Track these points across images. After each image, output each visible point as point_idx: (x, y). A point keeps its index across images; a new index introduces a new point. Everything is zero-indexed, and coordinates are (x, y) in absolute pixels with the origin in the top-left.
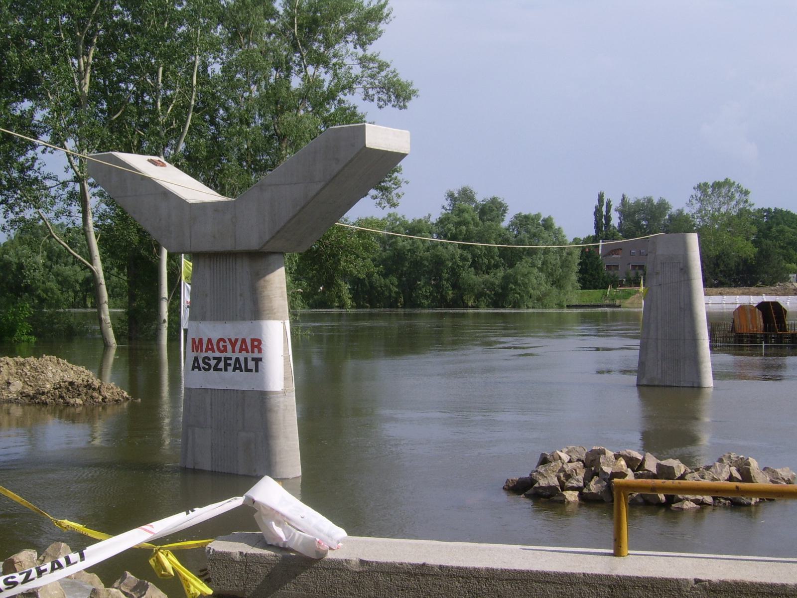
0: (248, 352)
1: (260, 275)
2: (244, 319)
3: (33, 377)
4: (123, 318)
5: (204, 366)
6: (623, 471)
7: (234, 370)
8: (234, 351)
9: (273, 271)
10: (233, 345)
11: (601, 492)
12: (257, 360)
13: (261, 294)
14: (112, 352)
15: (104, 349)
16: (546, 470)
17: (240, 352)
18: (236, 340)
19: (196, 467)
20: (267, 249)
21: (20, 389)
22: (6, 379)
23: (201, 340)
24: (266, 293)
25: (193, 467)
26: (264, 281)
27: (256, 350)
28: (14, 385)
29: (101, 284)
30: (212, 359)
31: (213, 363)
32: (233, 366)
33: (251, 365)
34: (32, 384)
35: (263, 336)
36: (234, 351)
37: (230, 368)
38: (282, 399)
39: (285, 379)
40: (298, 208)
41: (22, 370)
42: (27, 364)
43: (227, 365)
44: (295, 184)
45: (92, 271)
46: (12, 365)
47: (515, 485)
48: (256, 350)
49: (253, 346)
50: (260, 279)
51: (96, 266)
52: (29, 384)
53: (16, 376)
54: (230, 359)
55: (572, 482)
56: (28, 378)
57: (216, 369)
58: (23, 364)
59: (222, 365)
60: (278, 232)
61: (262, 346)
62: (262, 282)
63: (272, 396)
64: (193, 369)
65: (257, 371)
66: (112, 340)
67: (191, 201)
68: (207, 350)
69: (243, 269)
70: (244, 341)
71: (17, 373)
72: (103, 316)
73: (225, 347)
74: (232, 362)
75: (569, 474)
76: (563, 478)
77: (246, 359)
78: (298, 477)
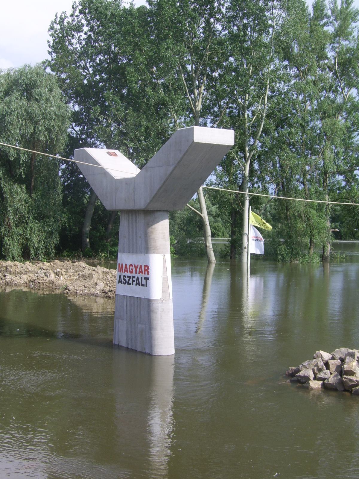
0: (142, 274)
1: (149, 225)
2: (141, 253)
3: (112, 281)
4: (228, 246)
5: (123, 281)
6: (352, 370)
7: (136, 285)
8: (136, 273)
9: (158, 222)
10: (136, 269)
11: (336, 383)
12: (147, 279)
13: (150, 237)
14: (213, 266)
15: (208, 264)
16: (308, 364)
17: (139, 273)
18: (138, 265)
19: (120, 344)
20: (152, 207)
21: (102, 288)
22: (96, 281)
23: (122, 264)
24: (153, 236)
25: (118, 344)
26: (152, 229)
27: (146, 272)
28: (99, 285)
29: (206, 225)
30: (127, 277)
31: (127, 279)
32: (136, 281)
33: (144, 282)
34: (110, 285)
35: (150, 263)
36: (136, 273)
37: (135, 283)
38: (160, 305)
39: (163, 292)
40: (162, 182)
41: (107, 277)
42: (109, 273)
43: (133, 281)
44: (161, 166)
45: (201, 216)
46: (101, 273)
47: (293, 373)
48: (146, 272)
49: (145, 270)
50: (150, 227)
51: (204, 214)
52: (109, 285)
53: (102, 280)
54: (134, 277)
55: (321, 374)
56: (109, 282)
57: (129, 284)
58: (107, 273)
59: (131, 281)
60: (154, 197)
61: (149, 270)
62: (150, 229)
63: (154, 302)
64: (119, 283)
65: (146, 286)
66: (213, 258)
67: (116, 178)
68: (125, 271)
69: (141, 220)
70: (141, 266)
71: (103, 278)
72: (208, 244)
73: (132, 269)
74: (135, 279)
75: (321, 369)
76: (316, 371)
77: (142, 278)
78: (173, 355)
